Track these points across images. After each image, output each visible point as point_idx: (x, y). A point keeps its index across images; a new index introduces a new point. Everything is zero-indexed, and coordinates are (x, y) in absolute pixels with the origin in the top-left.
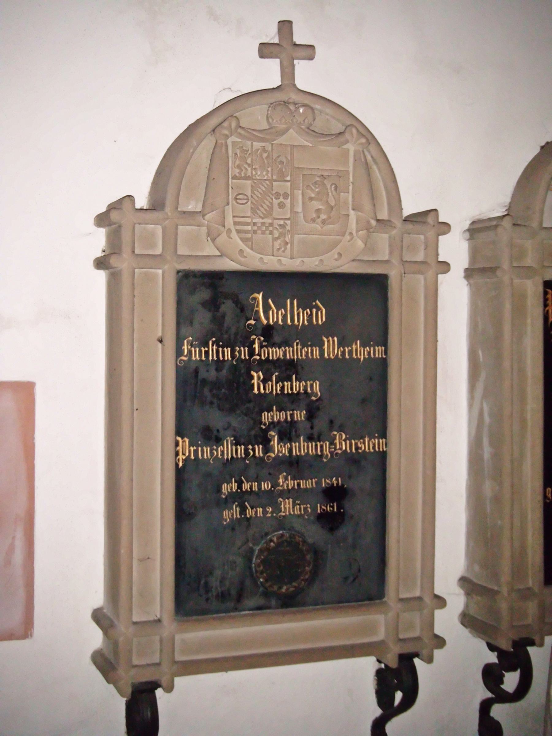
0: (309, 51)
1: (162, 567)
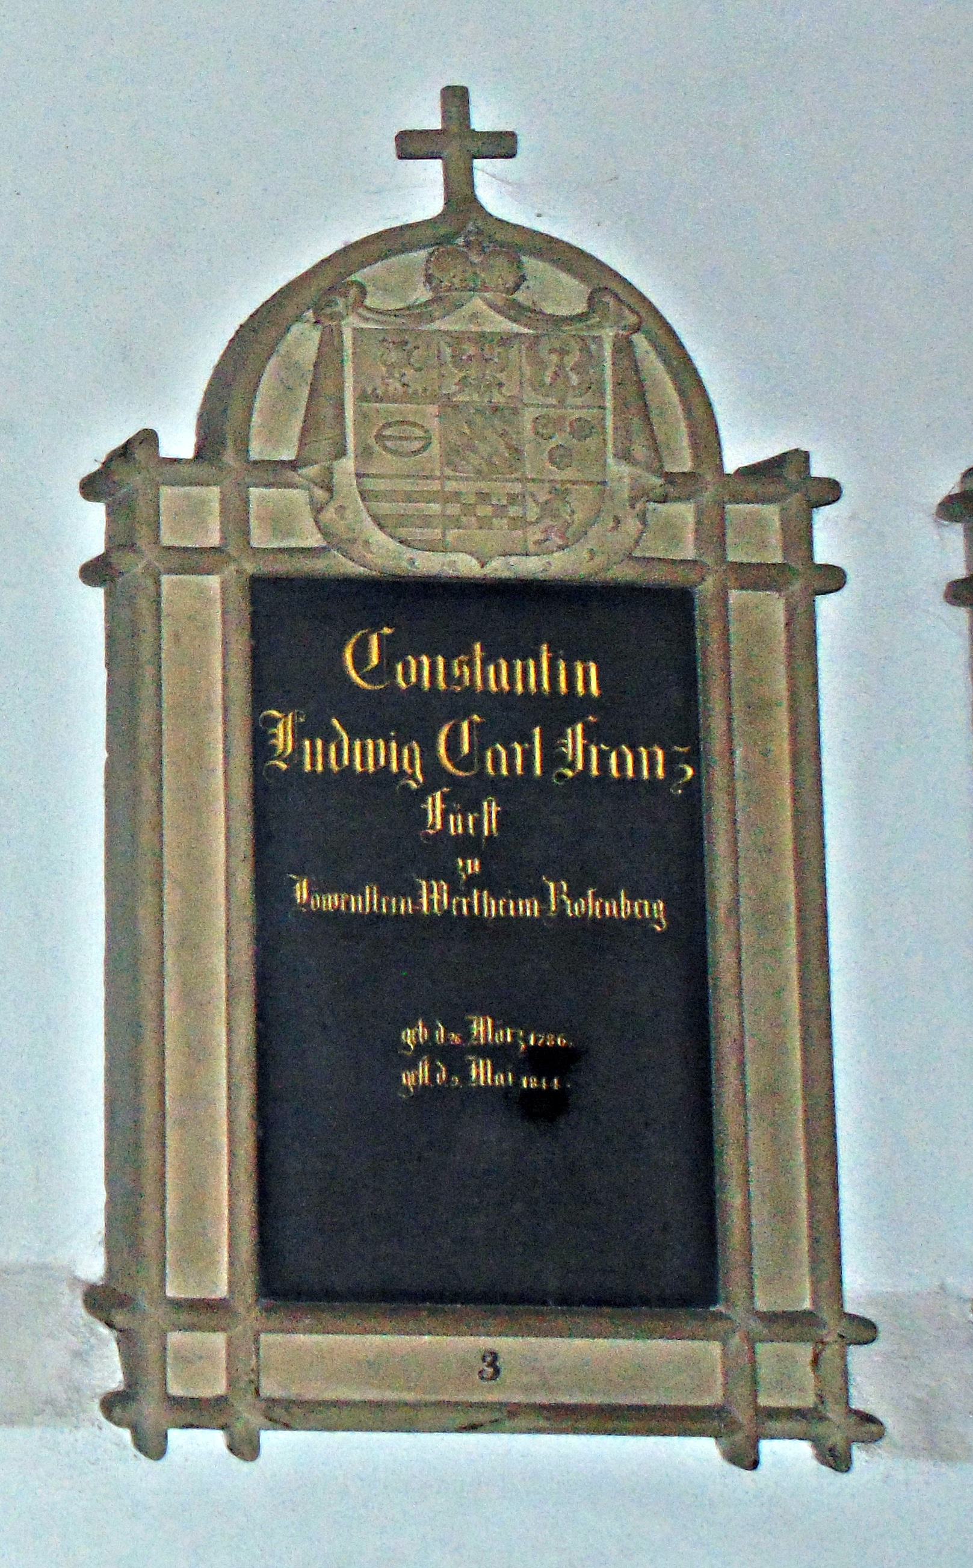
0: (503, 145)
1: (231, 1246)
